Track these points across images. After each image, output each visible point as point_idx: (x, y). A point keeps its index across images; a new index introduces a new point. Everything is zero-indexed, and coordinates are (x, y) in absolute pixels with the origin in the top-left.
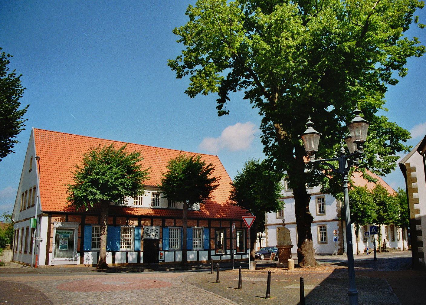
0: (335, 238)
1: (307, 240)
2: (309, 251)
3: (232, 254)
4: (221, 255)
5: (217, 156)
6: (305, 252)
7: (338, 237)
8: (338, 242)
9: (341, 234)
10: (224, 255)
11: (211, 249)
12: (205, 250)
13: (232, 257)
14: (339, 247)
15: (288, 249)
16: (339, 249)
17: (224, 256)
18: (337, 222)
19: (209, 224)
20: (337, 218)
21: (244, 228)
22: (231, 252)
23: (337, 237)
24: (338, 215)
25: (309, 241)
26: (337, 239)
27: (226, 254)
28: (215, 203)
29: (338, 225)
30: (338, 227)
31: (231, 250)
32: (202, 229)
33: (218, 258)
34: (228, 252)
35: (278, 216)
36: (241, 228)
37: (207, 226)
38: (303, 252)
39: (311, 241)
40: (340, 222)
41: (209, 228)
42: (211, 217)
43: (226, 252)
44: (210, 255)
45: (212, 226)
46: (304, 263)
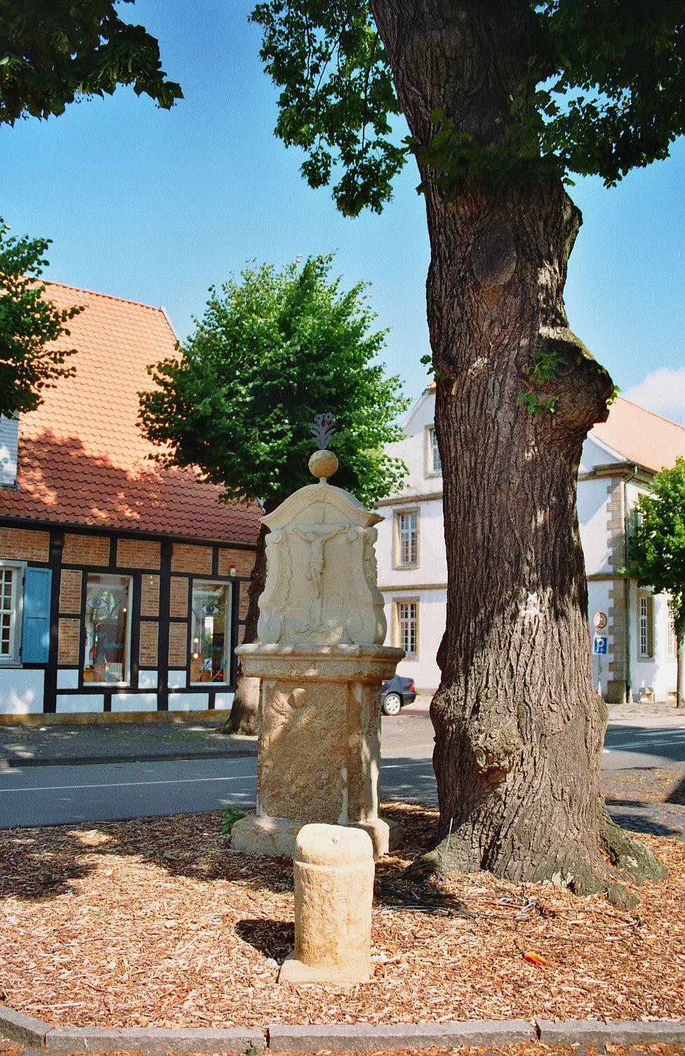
0: (599, 641)
1: (533, 607)
2: (555, 722)
3: (163, 692)
4: (108, 693)
5: (163, 309)
6: (511, 722)
7: (611, 640)
8: (609, 657)
9: (623, 628)
10: (127, 690)
11: (60, 662)
12: (28, 666)
13: (163, 703)
14: (610, 676)
15: (350, 684)
16: (609, 682)
17: (122, 696)
18: (609, 585)
19: (56, 549)
20: (610, 569)
21: (228, 578)
22: (163, 679)
23: (605, 640)
24: (611, 560)
25: (559, 614)
26: (604, 647)
27: (134, 689)
28: (99, 463)
29: (612, 594)
30: (611, 603)
31: (163, 670)
32: (18, 568)
33: (94, 703)
34: (148, 679)
35: (398, 563)
36: (215, 576)
37: (44, 556)
38: (494, 731)
39: (573, 613)
40: (621, 584)
41: (55, 564)
42: (62, 519)
43: (135, 679)
44: (51, 692)
45: (66, 559)
46: (494, 846)
